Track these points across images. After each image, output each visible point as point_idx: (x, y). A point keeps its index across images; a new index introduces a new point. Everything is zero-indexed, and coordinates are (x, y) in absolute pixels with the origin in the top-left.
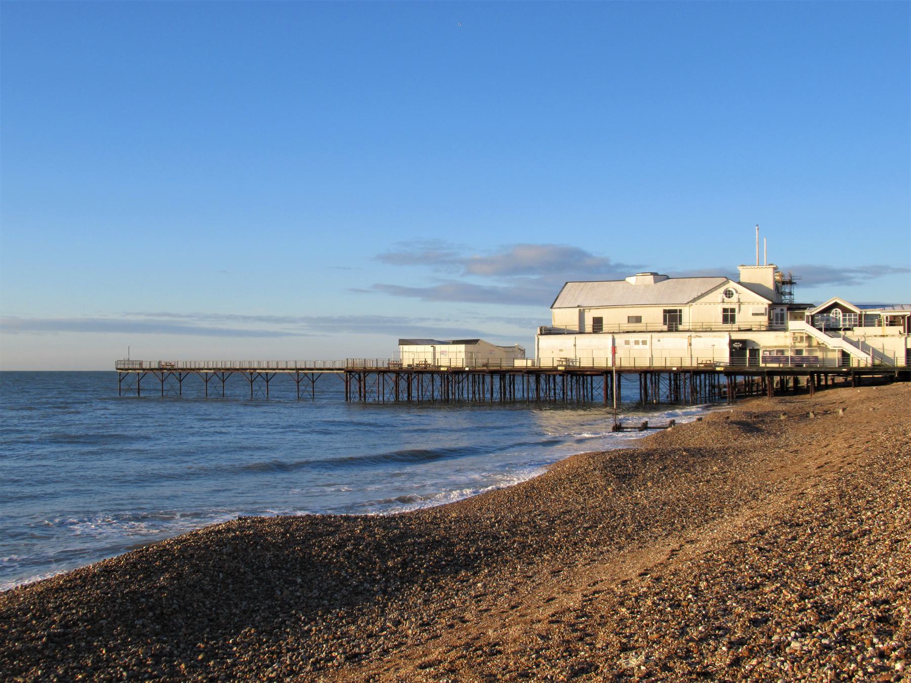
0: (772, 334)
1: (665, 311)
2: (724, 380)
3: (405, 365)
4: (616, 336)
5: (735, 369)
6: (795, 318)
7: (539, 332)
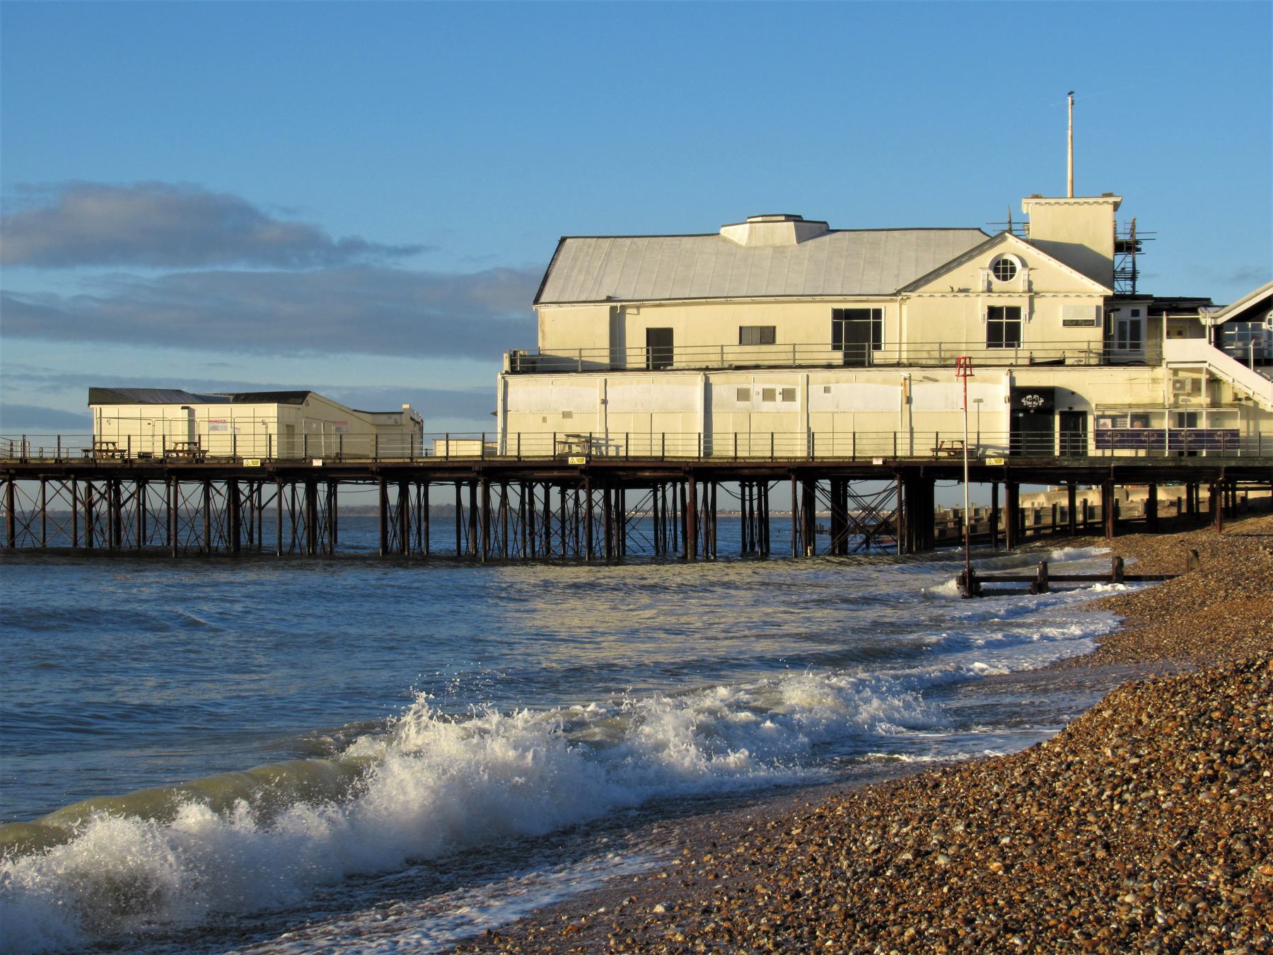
1: (837, 314)
4: (715, 378)
6: (1178, 331)
7: (506, 365)
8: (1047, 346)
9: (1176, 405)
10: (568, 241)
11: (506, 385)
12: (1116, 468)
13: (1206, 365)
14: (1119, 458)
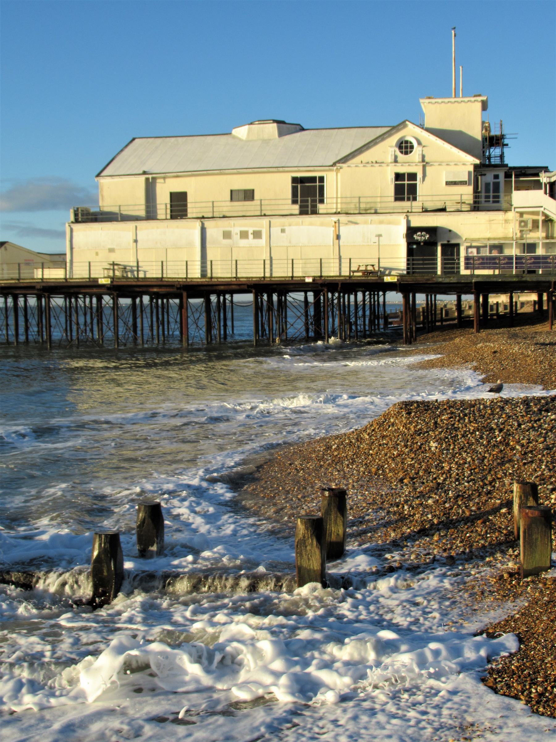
0: (482, 217)
2: (394, 298)
4: (207, 223)
5: (419, 278)
7: (72, 218)
8: (435, 198)
9: (522, 238)
10: (136, 140)
11: (72, 231)
12: (476, 283)
13: (542, 209)
14: (478, 276)
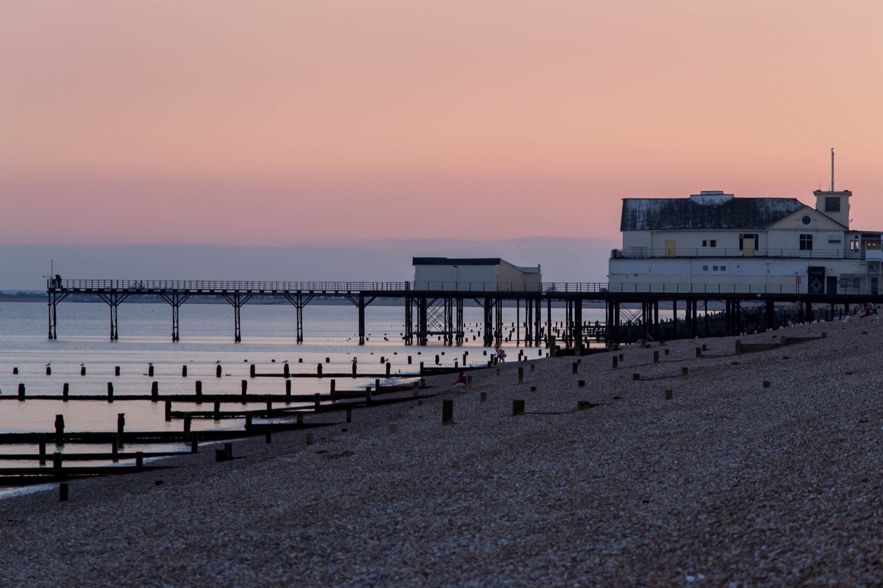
3: (545, 289)
